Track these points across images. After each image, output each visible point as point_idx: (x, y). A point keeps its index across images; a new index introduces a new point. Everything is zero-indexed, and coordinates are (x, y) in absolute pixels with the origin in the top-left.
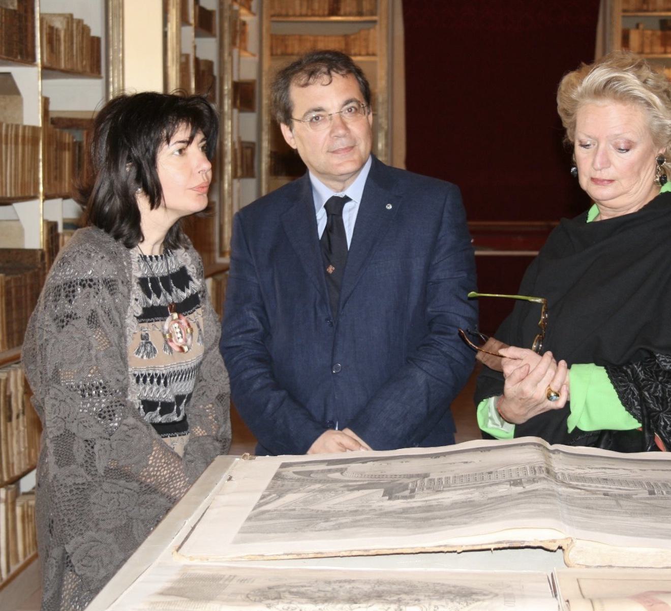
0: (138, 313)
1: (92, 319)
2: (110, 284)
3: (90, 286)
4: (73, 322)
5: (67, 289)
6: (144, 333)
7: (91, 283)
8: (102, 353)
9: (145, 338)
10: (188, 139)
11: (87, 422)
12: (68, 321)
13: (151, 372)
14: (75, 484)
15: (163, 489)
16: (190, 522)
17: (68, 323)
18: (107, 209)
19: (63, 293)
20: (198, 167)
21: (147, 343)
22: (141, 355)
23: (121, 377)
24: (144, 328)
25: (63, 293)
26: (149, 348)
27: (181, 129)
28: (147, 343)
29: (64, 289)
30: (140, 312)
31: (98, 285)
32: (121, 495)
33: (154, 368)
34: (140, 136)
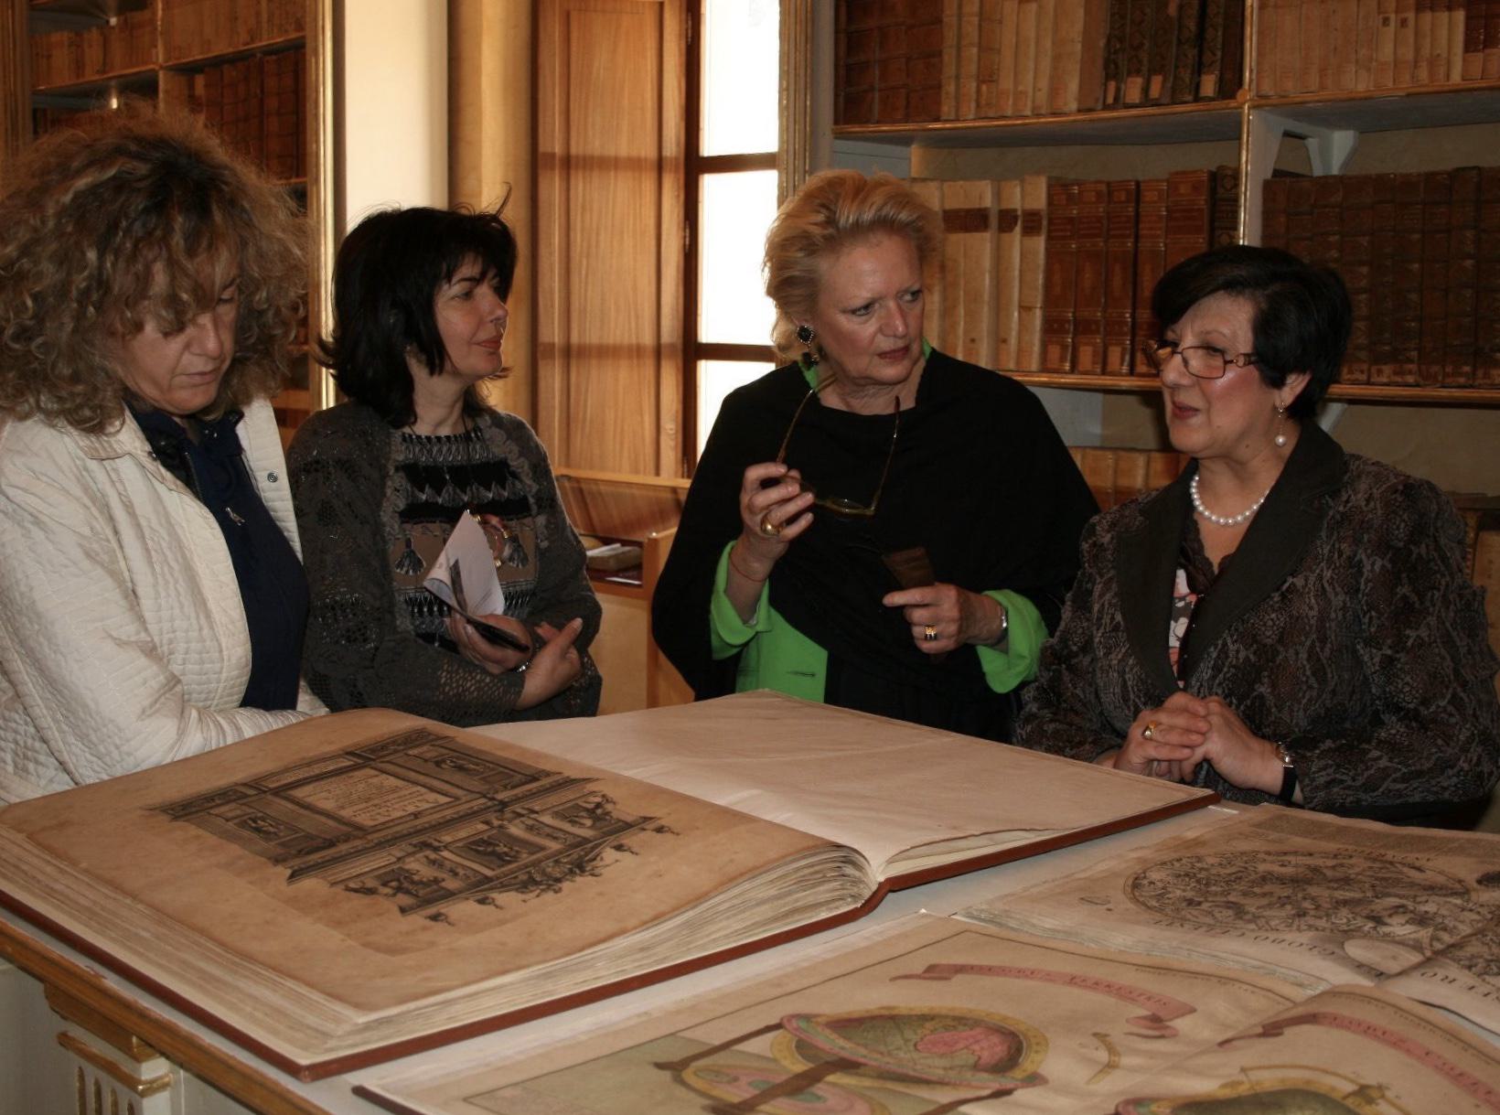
10: (478, 276)
11: (363, 635)
16: (112, 982)
18: (370, 374)
20: (491, 313)
22: (405, 569)
27: (466, 260)
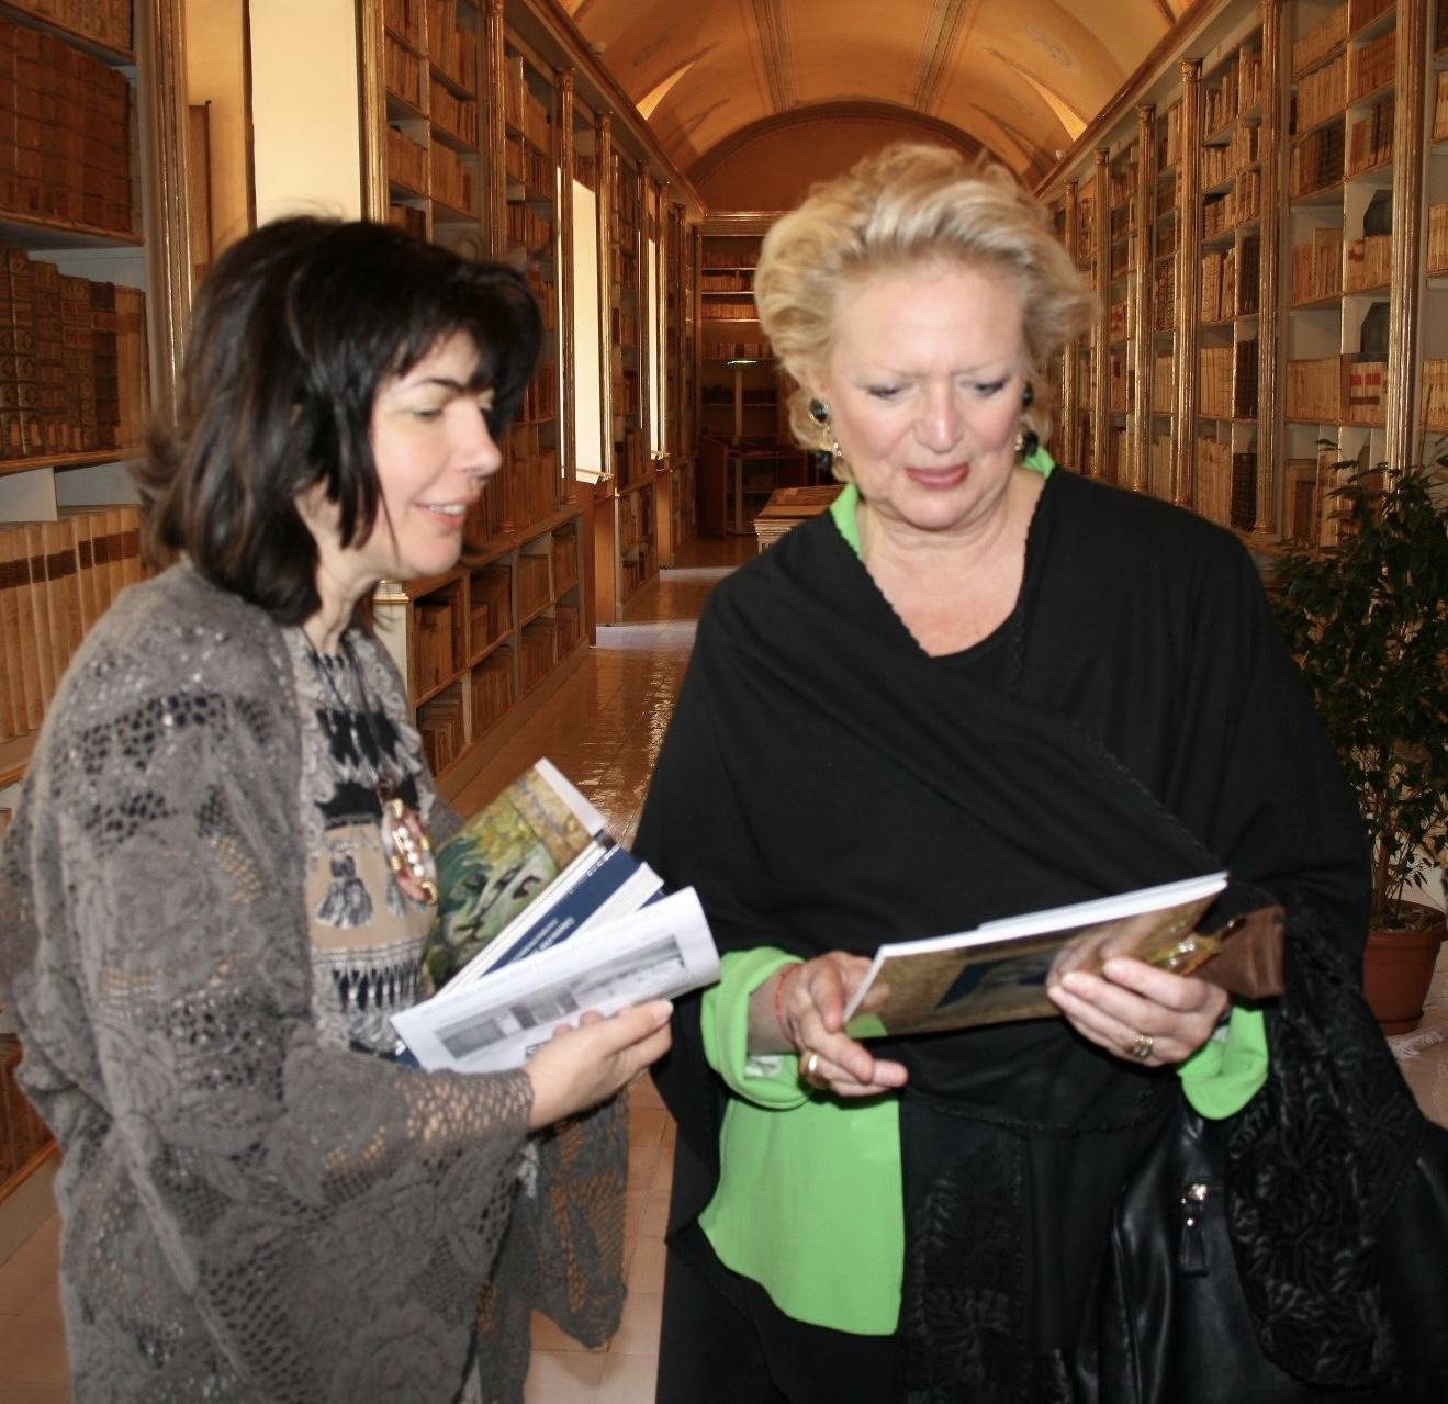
0: (324, 795)
1: (212, 813)
2: (255, 715)
3: (200, 719)
4: (153, 826)
5: (130, 733)
6: (339, 858)
7: (203, 712)
8: (247, 911)
9: (344, 869)
12: (135, 825)
13: (360, 965)
14: (258, 1249)
15: (477, 1124)
17: (137, 831)
19: (115, 746)
21: (349, 884)
22: (335, 917)
23: (298, 977)
24: (339, 841)
25: (115, 746)
26: (356, 898)
28: (349, 884)
29: (120, 733)
30: (329, 793)
31: (224, 716)
32: (392, 1215)
33: (369, 954)
34: (339, 339)
